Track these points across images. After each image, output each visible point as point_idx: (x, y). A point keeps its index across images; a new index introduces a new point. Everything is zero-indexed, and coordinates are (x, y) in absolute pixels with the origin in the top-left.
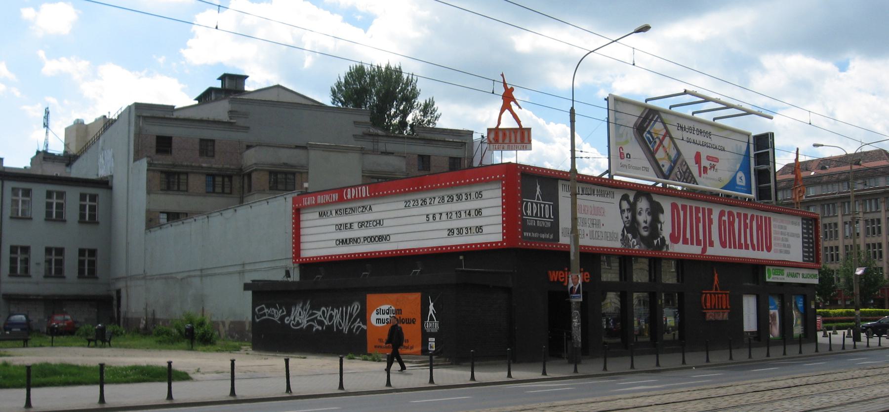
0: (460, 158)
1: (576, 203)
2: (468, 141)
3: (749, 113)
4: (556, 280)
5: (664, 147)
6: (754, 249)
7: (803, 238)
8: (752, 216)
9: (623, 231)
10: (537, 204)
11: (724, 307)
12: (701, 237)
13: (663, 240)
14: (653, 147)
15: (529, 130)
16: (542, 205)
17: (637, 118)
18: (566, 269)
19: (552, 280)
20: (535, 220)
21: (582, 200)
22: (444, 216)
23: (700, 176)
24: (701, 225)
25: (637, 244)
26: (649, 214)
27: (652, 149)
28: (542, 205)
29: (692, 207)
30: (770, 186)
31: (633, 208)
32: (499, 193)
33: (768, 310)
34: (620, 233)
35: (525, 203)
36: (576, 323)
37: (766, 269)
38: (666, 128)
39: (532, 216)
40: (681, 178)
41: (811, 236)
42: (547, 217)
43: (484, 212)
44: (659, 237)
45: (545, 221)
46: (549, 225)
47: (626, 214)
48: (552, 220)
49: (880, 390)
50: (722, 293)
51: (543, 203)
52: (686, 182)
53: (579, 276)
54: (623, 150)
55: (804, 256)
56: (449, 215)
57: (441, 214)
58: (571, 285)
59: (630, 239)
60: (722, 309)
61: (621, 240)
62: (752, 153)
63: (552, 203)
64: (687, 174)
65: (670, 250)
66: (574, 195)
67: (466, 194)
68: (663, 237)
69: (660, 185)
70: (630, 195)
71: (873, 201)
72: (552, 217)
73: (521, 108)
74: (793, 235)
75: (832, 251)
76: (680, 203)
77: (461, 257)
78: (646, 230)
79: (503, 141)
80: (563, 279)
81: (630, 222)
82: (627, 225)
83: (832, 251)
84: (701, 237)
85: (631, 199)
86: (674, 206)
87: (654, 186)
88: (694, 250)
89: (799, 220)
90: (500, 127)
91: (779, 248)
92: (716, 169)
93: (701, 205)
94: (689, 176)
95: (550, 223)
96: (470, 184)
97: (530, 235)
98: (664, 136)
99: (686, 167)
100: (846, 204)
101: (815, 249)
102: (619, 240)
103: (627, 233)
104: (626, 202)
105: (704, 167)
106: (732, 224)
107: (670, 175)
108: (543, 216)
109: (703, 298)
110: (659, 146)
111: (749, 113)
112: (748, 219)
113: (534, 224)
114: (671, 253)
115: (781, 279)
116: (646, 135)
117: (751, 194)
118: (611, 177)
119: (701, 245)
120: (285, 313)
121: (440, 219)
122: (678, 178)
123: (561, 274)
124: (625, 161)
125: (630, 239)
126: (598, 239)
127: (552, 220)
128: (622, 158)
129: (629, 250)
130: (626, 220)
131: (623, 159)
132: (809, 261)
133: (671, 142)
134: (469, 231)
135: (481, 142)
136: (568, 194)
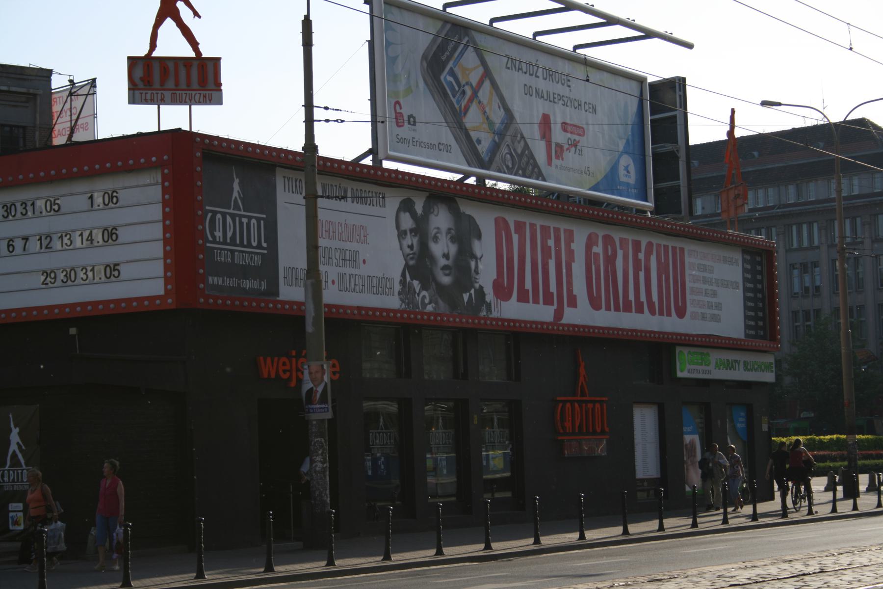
0: (24, 128)
1: (315, 216)
2: (41, 92)
3: (649, 34)
4: (273, 376)
5: (480, 102)
6: (652, 312)
7: (745, 289)
8: (650, 244)
9: (403, 275)
10: (233, 217)
11: (599, 430)
12: (553, 288)
13: (481, 292)
14: (458, 102)
15: (216, 61)
16: (245, 220)
17: (433, 36)
18: (294, 353)
19: (266, 375)
20: (230, 250)
21: (327, 210)
22: (34, 245)
23: (550, 163)
24: (552, 264)
25: (430, 303)
26: (453, 240)
27: (457, 106)
28: (245, 220)
29: (535, 225)
30: (679, 186)
31: (421, 229)
32: (156, 192)
33: (681, 435)
34: (397, 278)
35: (210, 215)
36: (320, 464)
37: (677, 352)
38: (484, 63)
39: (224, 242)
40: (513, 165)
41: (759, 286)
42: (255, 244)
43: (124, 235)
44: (473, 287)
45: (22, 485)
46: (258, 260)
47: (408, 240)
48: (265, 252)
49: (823, 582)
50: (594, 402)
51: (245, 216)
52: (524, 176)
53: (325, 367)
54: (401, 108)
55: (747, 327)
56: (45, 243)
57: (26, 239)
58: (307, 385)
59: (417, 291)
60: (594, 433)
61: (399, 293)
62: (649, 118)
63: (264, 216)
64: (525, 159)
65: (495, 314)
66: (311, 199)
67: (24, 204)
68: (481, 287)
69: (472, 181)
70: (414, 199)
71: (805, 227)
72: (265, 245)
73: (199, 17)
74: (725, 284)
75: (808, 320)
76: (512, 218)
77: (73, 331)
78: (447, 272)
79: (162, 83)
80: (288, 374)
81: (416, 256)
82: (412, 263)
83: (808, 320)
84: (553, 288)
85: (419, 208)
86: (501, 226)
87: (461, 181)
88: (543, 313)
89: (738, 256)
90: (155, 54)
91: (700, 311)
92: (581, 151)
93: (552, 223)
94: (527, 163)
95: (260, 257)
96: (38, 182)
97: (220, 282)
98: (481, 82)
99: (522, 143)
100: (794, 228)
101: (767, 311)
102: (396, 293)
103: (412, 279)
104: (408, 214)
105: (557, 145)
106: (610, 260)
107: (491, 161)
108: (245, 243)
109: (559, 409)
110: (471, 100)
111: (649, 34)
112: (640, 252)
113: (229, 260)
114: (497, 320)
115: (704, 372)
116: (445, 77)
117: (646, 200)
118: (377, 162)
119: (552, 304)
120: (369, 453)
121: (24, 250)
122: (507, 167)
123: (284, 364)
124: (405, 131)
125: (417, 291)
126: (354, 291)
127: (265, 252)
128: (399, 125)
129: (416, 314)
130: (408, 251)
131: (402, 126)
132: (756, 336)
133: (494, 93)
134: (90, 274)
135: (71, 94)
136: (300, 199)
